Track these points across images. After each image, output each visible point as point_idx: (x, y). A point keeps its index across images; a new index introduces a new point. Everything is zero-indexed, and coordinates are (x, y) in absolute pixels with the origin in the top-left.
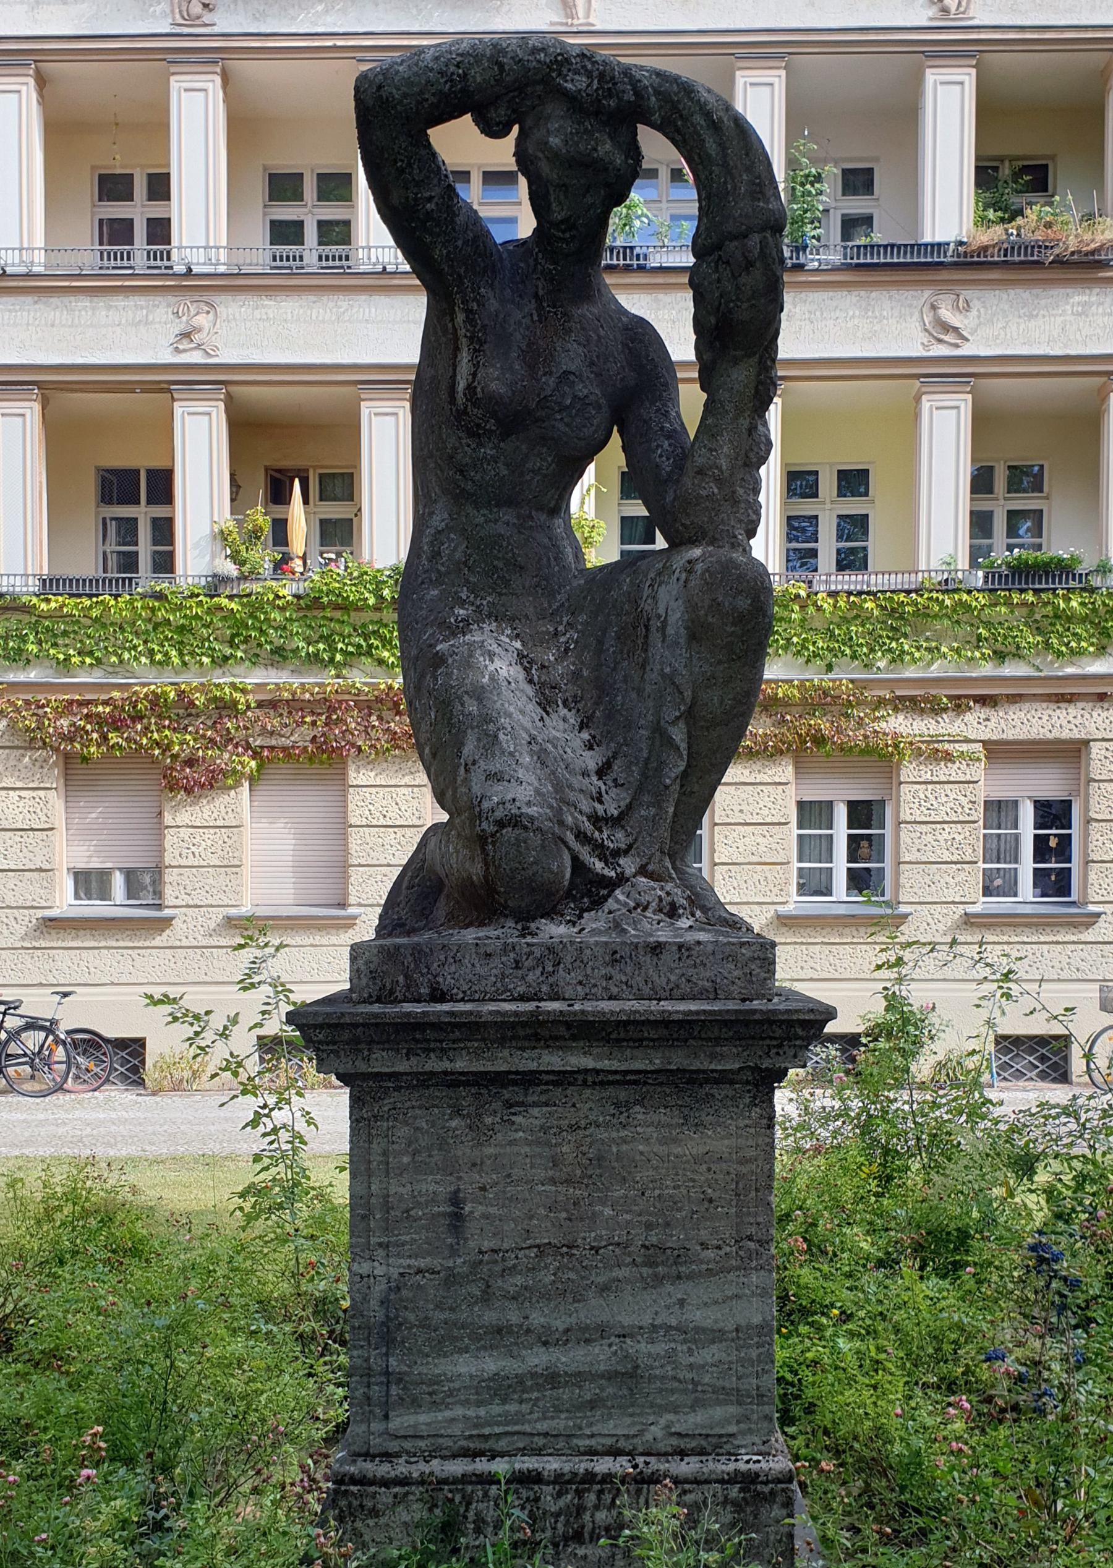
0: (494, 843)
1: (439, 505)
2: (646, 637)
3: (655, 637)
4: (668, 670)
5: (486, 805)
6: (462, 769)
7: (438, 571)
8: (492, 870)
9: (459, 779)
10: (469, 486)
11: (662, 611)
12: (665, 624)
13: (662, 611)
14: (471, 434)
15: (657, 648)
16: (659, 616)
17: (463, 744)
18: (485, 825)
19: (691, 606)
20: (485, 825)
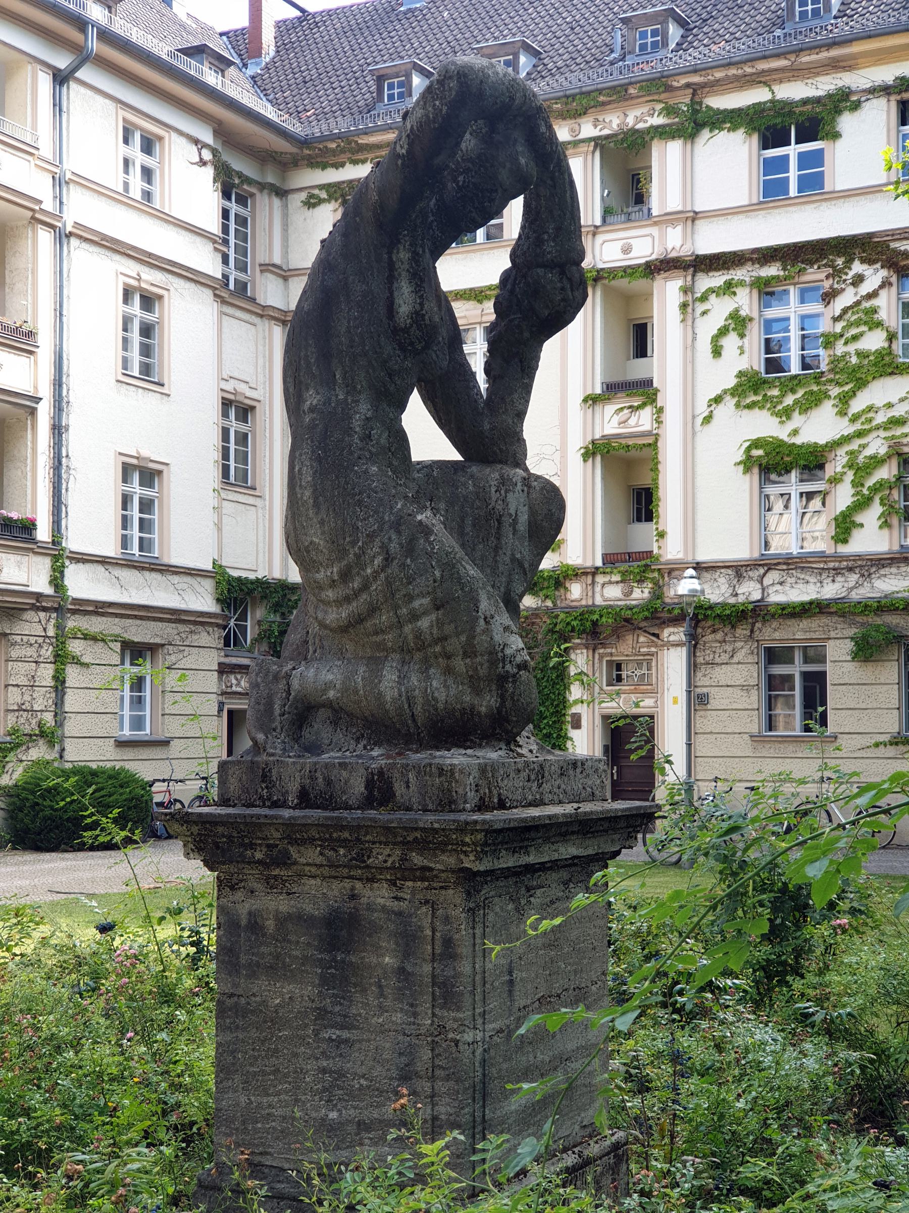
0: (514, 682)
1: (362, 397)
2: (499, 528)
3: (507, 530)
4: (518, 556)
5: (508, 652)
6: (482, 622)
7: (370, 451)
8: (508, 704)
9: (478, 630)
10: (392, 388)
11: (512, 512)
12: (515, 522)
13: (512, 512)
14: (402, 348)
15: (509, 539)
16: (511, 515)
17: (478, 601)
18: (508, 667)
19: (532, 513)
20: (508, 667)
